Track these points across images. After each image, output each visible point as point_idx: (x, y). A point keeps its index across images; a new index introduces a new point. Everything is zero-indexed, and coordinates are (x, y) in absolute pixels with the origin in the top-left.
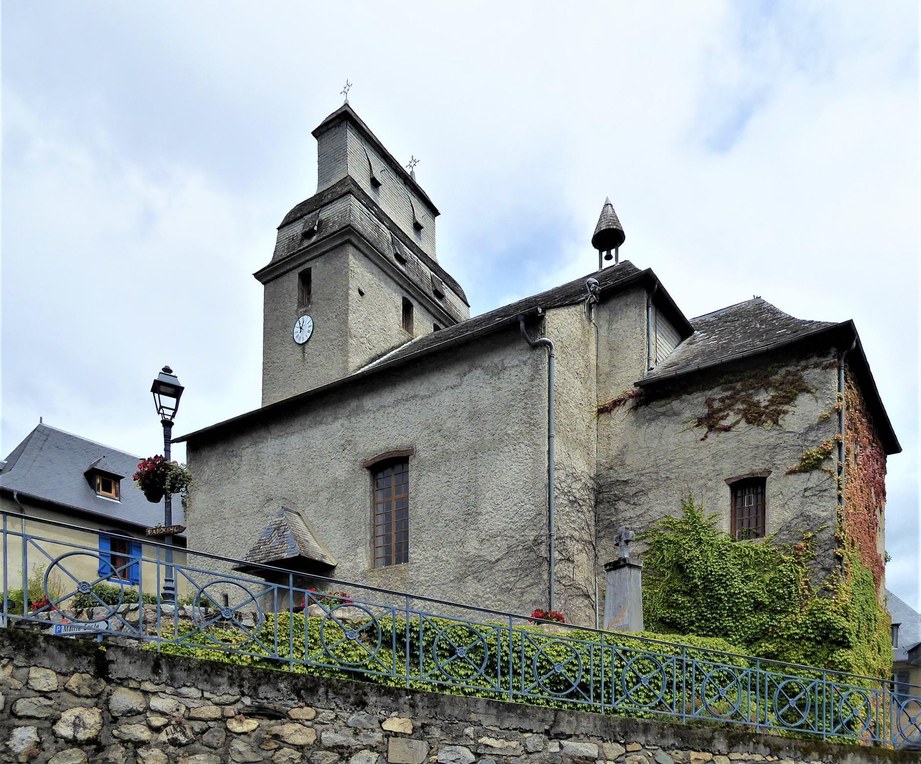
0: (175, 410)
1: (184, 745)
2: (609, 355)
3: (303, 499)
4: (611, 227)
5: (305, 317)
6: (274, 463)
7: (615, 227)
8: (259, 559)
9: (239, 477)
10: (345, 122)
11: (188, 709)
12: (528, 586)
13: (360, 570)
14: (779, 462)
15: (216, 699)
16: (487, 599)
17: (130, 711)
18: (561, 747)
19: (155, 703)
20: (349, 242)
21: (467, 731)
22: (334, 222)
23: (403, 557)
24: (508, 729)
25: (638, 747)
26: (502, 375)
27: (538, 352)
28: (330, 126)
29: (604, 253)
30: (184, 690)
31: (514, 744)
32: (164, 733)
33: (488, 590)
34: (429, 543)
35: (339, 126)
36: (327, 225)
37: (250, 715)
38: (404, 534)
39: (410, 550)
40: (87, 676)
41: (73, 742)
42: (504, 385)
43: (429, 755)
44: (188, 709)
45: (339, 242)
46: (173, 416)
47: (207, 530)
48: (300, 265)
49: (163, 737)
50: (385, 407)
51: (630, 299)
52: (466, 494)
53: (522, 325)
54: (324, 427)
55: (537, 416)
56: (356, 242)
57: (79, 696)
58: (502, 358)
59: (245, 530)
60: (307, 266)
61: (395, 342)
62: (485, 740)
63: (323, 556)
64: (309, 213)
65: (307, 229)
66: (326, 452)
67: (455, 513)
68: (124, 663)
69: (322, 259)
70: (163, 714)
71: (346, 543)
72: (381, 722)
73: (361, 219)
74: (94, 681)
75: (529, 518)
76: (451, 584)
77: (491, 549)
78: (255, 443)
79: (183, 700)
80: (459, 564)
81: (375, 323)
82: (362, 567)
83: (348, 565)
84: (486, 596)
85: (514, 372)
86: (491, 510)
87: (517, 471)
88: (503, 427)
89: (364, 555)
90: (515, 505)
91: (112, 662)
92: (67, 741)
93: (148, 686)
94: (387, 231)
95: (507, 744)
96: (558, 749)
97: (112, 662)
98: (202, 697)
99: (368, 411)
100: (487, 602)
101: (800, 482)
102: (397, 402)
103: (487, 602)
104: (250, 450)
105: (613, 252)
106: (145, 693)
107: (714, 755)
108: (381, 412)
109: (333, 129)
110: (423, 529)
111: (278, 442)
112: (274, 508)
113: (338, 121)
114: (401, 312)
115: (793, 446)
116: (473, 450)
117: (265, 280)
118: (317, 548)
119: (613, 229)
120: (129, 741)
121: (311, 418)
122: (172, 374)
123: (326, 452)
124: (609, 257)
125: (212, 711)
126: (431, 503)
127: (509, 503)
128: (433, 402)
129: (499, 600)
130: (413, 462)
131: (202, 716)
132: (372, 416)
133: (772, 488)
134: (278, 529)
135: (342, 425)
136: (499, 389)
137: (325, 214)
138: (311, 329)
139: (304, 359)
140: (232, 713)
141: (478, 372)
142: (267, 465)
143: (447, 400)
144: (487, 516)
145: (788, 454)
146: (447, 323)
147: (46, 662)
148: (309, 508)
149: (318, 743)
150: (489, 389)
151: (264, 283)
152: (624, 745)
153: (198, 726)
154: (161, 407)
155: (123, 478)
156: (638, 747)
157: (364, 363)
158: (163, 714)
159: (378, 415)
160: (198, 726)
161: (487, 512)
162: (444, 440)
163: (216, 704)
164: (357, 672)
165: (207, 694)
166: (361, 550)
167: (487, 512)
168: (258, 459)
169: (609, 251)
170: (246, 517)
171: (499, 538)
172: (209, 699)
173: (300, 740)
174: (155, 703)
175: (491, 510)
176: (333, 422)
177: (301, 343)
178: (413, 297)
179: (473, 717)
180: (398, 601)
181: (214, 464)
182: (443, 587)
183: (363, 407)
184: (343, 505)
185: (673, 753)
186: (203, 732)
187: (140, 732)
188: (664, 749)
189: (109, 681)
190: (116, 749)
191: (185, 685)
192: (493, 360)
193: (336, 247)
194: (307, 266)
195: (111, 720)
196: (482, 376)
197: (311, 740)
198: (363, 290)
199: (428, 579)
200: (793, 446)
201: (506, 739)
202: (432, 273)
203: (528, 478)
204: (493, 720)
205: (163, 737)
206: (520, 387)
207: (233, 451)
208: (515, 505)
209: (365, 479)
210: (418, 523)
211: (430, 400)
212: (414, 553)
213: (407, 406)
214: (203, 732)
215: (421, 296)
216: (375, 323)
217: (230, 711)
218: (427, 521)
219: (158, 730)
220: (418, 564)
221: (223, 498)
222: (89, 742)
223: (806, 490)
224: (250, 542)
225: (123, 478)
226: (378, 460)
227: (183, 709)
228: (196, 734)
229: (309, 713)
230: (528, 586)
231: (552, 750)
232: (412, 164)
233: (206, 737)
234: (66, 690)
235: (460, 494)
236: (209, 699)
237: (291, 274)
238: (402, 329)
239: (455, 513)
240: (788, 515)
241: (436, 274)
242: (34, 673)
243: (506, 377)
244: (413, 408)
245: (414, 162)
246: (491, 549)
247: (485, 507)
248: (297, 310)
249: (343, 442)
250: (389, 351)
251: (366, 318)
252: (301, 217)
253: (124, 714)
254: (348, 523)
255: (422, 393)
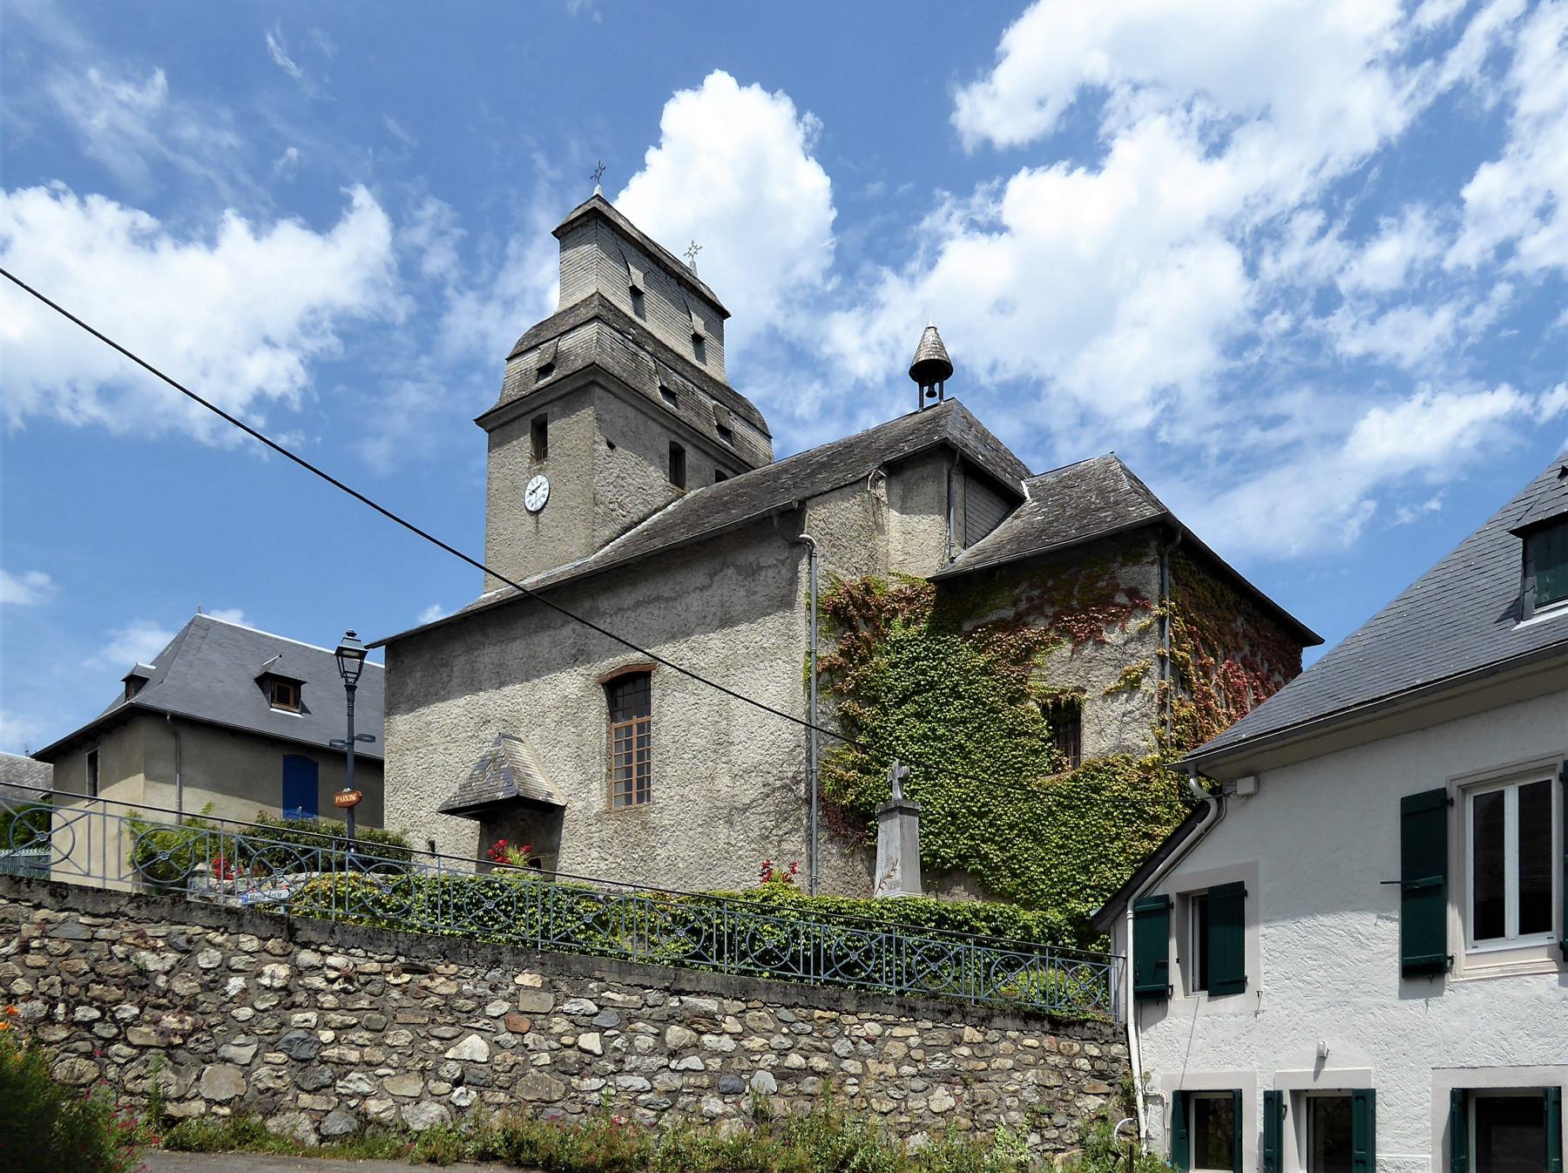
0: (359, 674)
1: (353, 993)
2: (902, 541)
3: (527, 721)
4: (932, 357)
5: (539, 477)
6: (492, 676)
7: (936, 357)
8: (469, 799)
9: (449, 692)
10: (593, 222)
11: (355, 965)
12: (786, 833)
13: (594, 811)
14: (1095, 679)
15: (377, 957)
16: (740, 848)
17: (312, 966)
18: (680, 1001)
19: (331, 960)
20: (594, 383)
21: (591, 986)
22: (577, 355)
23: (644, 796)
24: (629, 985)
25: (760, 1005)
26: (757, 575)
27: (797, 550)
28: (575, 225)
29: (926, 389)
30: (353, 951)
31: (635, 998)
32: (337, 983)
33: (742, 837)
34: (674, 778)
35: (586, 225)
36: (567, 358)
37: (406, 971)
38: (644, 768)
39: (653, 787)
40: (281, 940)
41: (269, 988)
42: (759, 588)
43: (555, 1005)
44: (355, 965)
45: (582, 383)
46: (356, 679)
47: (410, 758)
48: (534, 410)
49: (336, 987)
50: (624, 610)
51: (928, 469)
52: (716, 719)
53: (775, 521)
54: (552, 632)
55: (796, 627)
56: (603, 383)
57: (274, 955)
58: (758, 555)
59: (457, 760)
60: (540, 412)
61: (659, 501)
62: (608, 994)
63: (550, 795)
64: (546, 341)
65: (544, 364)
66: (554, 663)
67: (704, 742)
68: (307, 930)
69: (560, 403)
70: (336, 969)
71: (578, 777)
72: (514, 977)
73: (612, 349)
74: (285, 944)
75: (787, 750)
76: (700, 830)
77: (745, 787)
78: (469, 650)
79: (351, 958)
80: (709, 805)
81: (631, 481)
82: (596, 806)
83: (579, 805)
84: (740, 845)
85: (770, 573)
86: (745, 739)
87: (775, 693)
88: (758, 639)
89: (598, 793)
90: (772, 733)
91: (299, 929)
92: (267, 988)
93: (325, 948)
94: (648, 357)
95: (628, 998)
96: (678, 1004)
97: (299, 929)
98: (366, 956)
99: (604, 614)
100: (740, 852)
101: (1119, 706)
102: (638, 604)
103: (740, 852)
104: (462, 659)
105: (937, 386)
106: (324, 953)
107: (841, 1014)
108: (619, 615)
109: (579, 229)
110: (667, 761)
111: (497, 649)
112: (491, 733)
113: (585, 219)
114: (668, 462)
115: (1109, 659)
116: (724, 665)
117: (489, 427)
118: (541, 784)
119: (934, 360)
120: (310, 989)
121: (537, 620)
122: (356, 638)
123: (554, 663)
124: (931, 394)
125: (373, 967)
126: (676, 729)
127: (765, 732)
128: (680, 606)
129: (753, 850)
130: (655, 680)
131: (366, 971)
132: (609, 620)
133: (1088, 712)
134: (494, 760)
135: (574, 631)
136: (755, 593)
137: (565, 344)
138: (546, 493)
139: (537, 531)
140: (389, 969)
141: (730, 572)
142: (484, 677)
143: (695, 604)
144: (740, 747)
145: (1105, 670)
146: (735, 467)
147: (251, 930)
148: (533, 733)
149: (460, 994)
150: (742, 593)
151: (488, 431)
152: (746, 1002)
153: (362, 979)
154: (345, 672)
155: (305, 682)
156: (760, 1005)
157: (615, 535)
158: (336, 969)
159: (617, 619)
160: (362, 979)
161: (740, 742)
162: (691, 653)
163: (377, 962)
164: (1165, 966)
165: (369, 954)
166: (595, 785)
167: (740, 742)
168: (472, 671)
169: (931, 387)
170: (458, 743)
171: (754, 774)
172: (372, 958)
173: (444, 990)
174: (331, 960)
175: (745, 739)
176: (563, 626)
177: (533, 509)
178: (685, 440)
179: (597, 974)
180: (638, 850)
181: (418, 675)
182: (691, 833)
183: (598, 608)
184: (573, 730)
185: (797, 1011)
186: (367, 983)
187: (317, 982)
188: (787, 1007)
189: (296, 943)
190: (302, 995)
191: (353, 947)
192: (748, 557)
193: (578, 389)
194: (540, 412)
195: (298, 972)
196: (734, 577)
197: (454, 991)
198: (613, 442)
199: (672, 822)
200: (1109, 659)
201: (629, 994)
202: (715, 402)
203: (786, 701)
204: (616, 977)
205: (336, 987)
206: (777, 592)
207: (442, 659)
208: (772, 733)
209: (599, 701)
210: (661, 754)
211: (676, 604)
212: (658, 791)
213: (649, 610)
214: (367, 983)
215: (698, 437)
216: (631, 481)
217: (388, 967)
218: (673, 751)
219: (331, 981)
220: (661, 805)
221: (429, 718)
222: (282, 988)
223: (1124, 715)
224: (462, 775)
225: (305, 682)
226: (615, 675)
227: (351, 966)
228: (362, 985)
229: (453, 968)
230: (786, 833)
231: (672, 1004)
232: (692, 252)
233: (369, 987)
234: (265, 951)
235: (709, 719)
236: (372, 958)
237: (522, 420)
238: (669, 484)
239: (704, 742)
240: (1105, 744)
241: (721, 403)
242: (243, 938)
243: (762, 578)
244: (656, 612)
245: (694, 249)
246: (745, 787)
247: (739, 735)
248: (530, 467)
249: (573, 652)
250: (650, 515)
251: (618, 477)
252: (536, 347)
253: (307, 968)
254: (580, 752)
255: (666, 595)
